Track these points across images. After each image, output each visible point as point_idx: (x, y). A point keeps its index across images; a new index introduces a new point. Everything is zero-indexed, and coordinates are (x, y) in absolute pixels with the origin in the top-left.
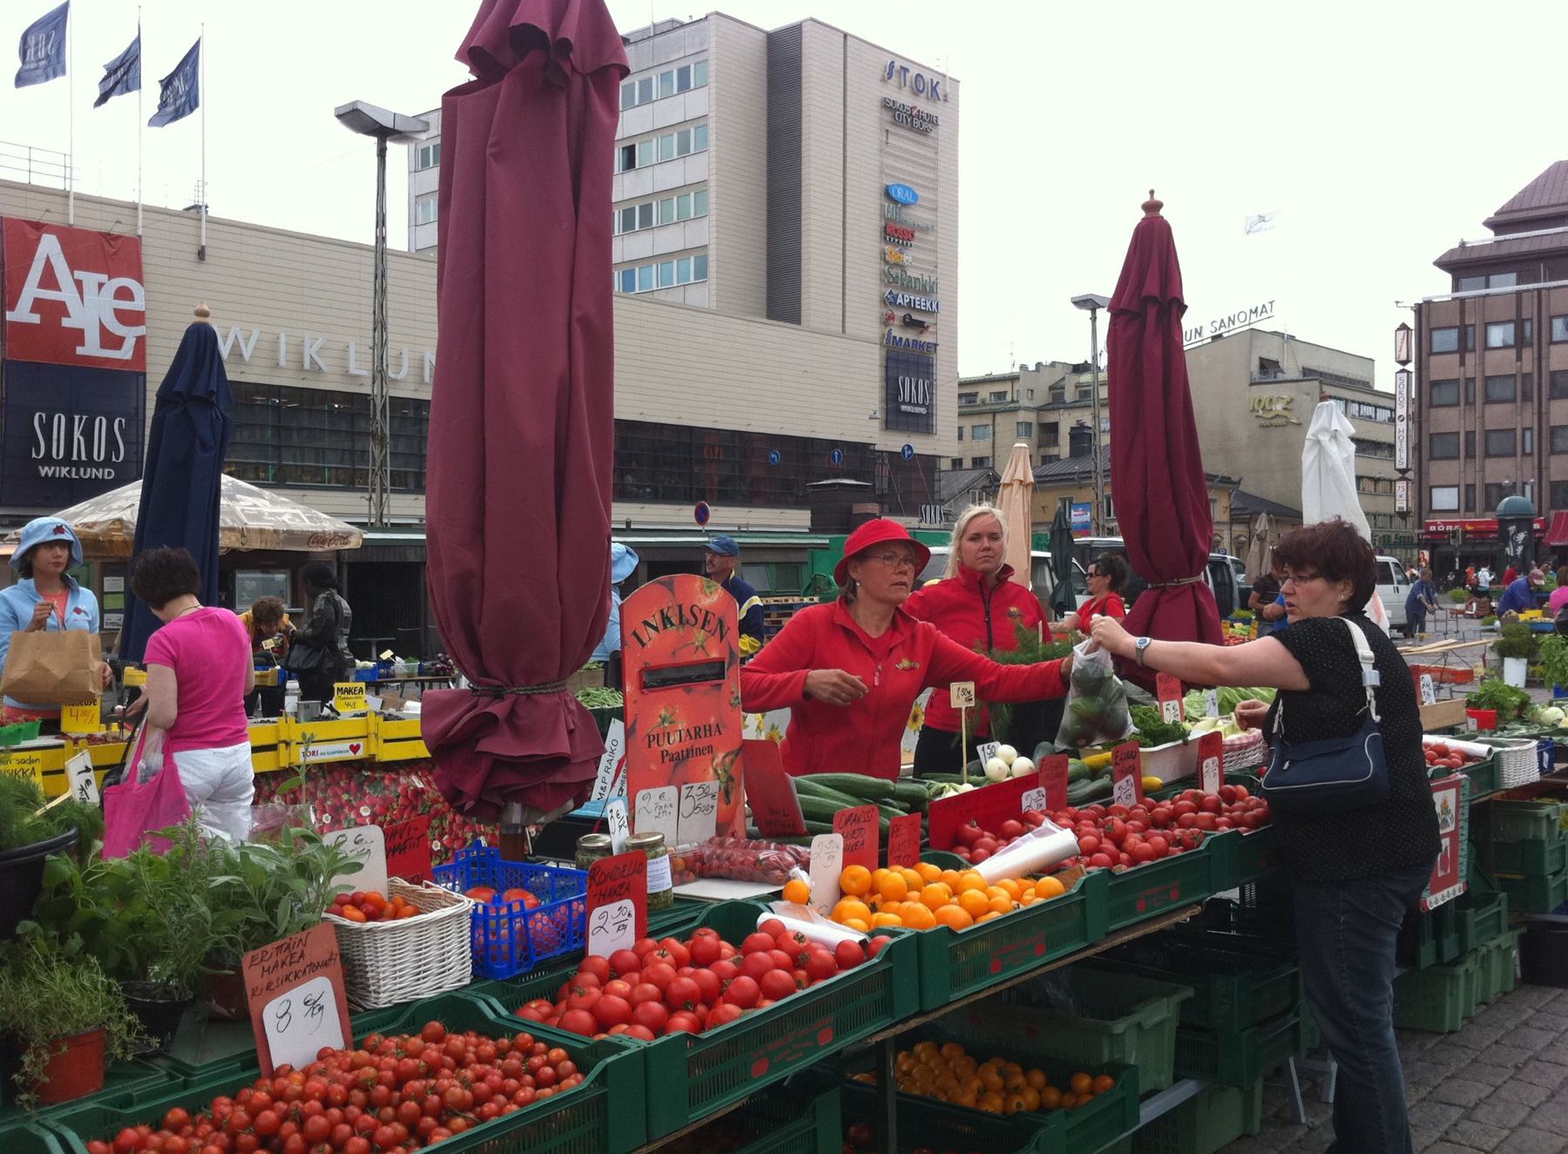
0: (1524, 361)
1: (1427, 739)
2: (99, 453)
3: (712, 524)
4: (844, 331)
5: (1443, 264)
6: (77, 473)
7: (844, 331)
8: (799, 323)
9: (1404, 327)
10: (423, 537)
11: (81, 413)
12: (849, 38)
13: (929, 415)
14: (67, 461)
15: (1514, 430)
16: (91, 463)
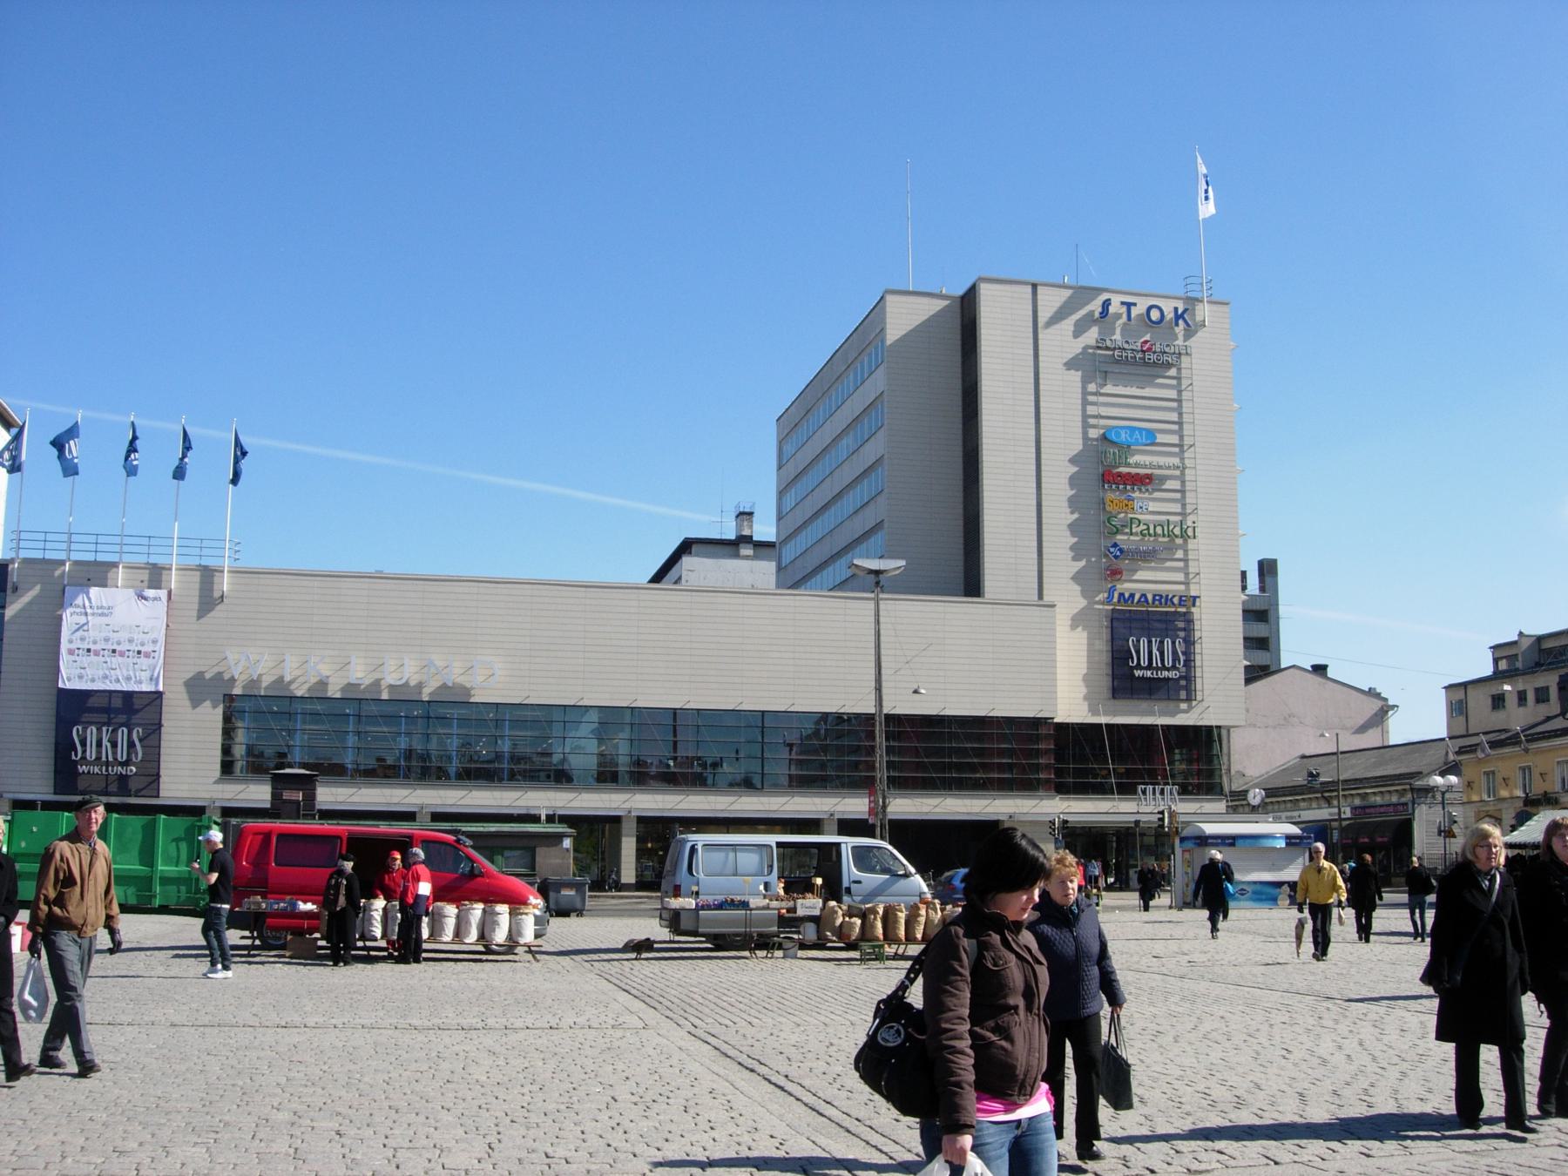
2: (1169, 662)
4: (1041, 596)
6: (107, 770)
7: (1041, 596)
13: (1188, 679)
14: (1150, 667)
16: (1164, 668)
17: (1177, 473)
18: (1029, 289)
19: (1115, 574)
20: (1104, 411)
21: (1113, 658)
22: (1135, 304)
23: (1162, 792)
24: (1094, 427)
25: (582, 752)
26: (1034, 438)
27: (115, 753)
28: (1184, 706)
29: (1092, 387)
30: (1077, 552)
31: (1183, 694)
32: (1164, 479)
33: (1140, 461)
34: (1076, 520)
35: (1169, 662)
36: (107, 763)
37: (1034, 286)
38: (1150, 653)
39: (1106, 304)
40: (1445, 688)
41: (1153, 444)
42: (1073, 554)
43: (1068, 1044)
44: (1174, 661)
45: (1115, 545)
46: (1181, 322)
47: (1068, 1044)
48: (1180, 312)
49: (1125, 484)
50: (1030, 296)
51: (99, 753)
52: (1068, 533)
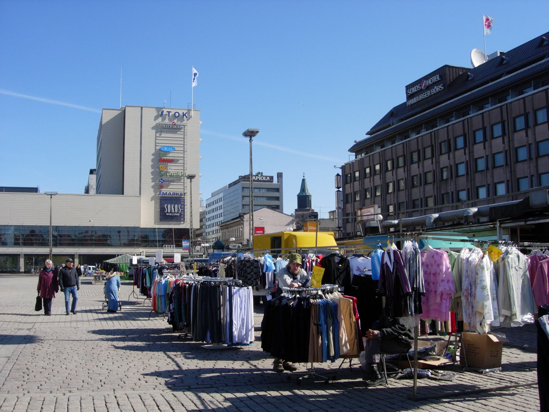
1: (533, 357)
3: (378, 225)
9: (338, 175)
11: (173, 204)
17: (183, 158)
18: (140, 108)
19: (162, 187)
20: (160, 142)
21: (160, 210)
22: (171, 112)
23: (170, 247)
24: (158, 146)
25: (10, 237)
26: (139, 150)
27: (175, 211)
28: (182, 222)
29: (158, 135)
30: (153, 180)
31: (182, 220)
32: (178, 160)
33: (170, 156)
34: (153, 171)
35: (176, 211)
36: (173, 213)
37: (142, 108)
38: (171, 209)
39: (163, 112)
40: (329, 212)
41: (175, 150)
42: (152, 180)
43: (360, 320)
44: (178, 211)
45: (162, 179)
46: (185, 116)
47: (360, 320)
48: (184, 113)
50: (140, 110)
51: (171, 211)
52: (151, 175)
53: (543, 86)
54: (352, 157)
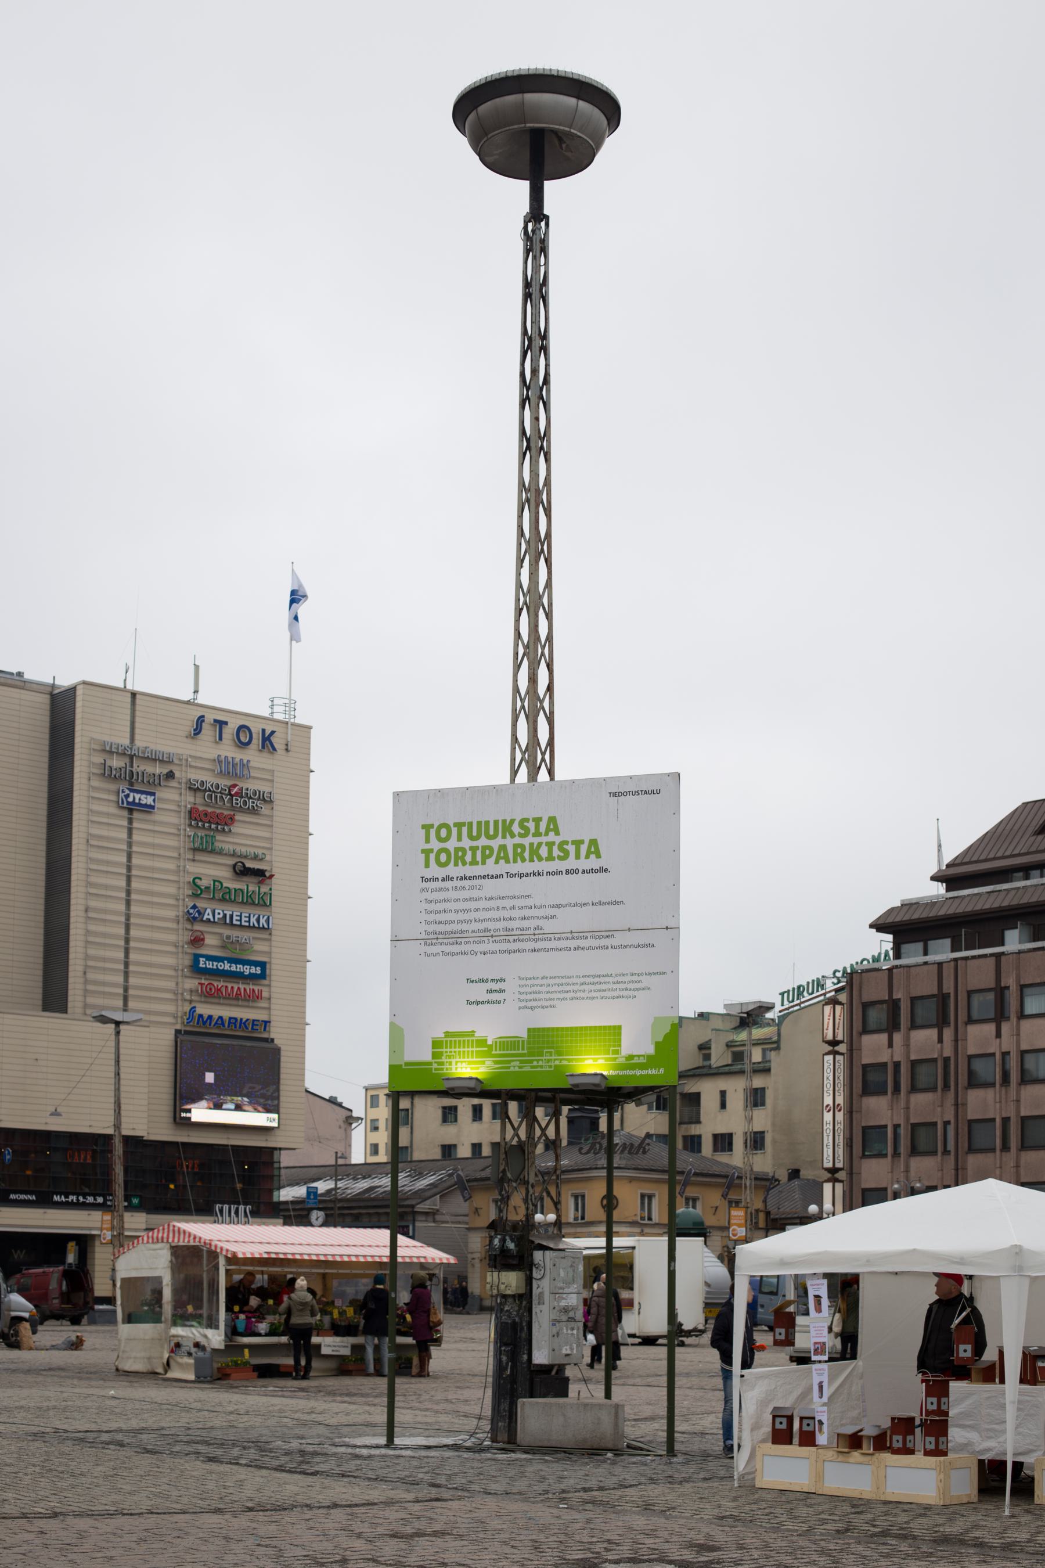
0: (1003, 1037)
5: (879, 926)
8: (65, 1011)
10: (849, 1345)
12: (138, 696)
15: (935, 1124)
23: (237, 1212)
49: (209, 822)
53: (1038, 940)
54: (525, 1035)
